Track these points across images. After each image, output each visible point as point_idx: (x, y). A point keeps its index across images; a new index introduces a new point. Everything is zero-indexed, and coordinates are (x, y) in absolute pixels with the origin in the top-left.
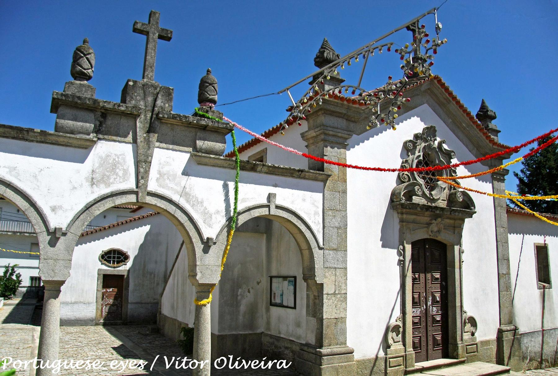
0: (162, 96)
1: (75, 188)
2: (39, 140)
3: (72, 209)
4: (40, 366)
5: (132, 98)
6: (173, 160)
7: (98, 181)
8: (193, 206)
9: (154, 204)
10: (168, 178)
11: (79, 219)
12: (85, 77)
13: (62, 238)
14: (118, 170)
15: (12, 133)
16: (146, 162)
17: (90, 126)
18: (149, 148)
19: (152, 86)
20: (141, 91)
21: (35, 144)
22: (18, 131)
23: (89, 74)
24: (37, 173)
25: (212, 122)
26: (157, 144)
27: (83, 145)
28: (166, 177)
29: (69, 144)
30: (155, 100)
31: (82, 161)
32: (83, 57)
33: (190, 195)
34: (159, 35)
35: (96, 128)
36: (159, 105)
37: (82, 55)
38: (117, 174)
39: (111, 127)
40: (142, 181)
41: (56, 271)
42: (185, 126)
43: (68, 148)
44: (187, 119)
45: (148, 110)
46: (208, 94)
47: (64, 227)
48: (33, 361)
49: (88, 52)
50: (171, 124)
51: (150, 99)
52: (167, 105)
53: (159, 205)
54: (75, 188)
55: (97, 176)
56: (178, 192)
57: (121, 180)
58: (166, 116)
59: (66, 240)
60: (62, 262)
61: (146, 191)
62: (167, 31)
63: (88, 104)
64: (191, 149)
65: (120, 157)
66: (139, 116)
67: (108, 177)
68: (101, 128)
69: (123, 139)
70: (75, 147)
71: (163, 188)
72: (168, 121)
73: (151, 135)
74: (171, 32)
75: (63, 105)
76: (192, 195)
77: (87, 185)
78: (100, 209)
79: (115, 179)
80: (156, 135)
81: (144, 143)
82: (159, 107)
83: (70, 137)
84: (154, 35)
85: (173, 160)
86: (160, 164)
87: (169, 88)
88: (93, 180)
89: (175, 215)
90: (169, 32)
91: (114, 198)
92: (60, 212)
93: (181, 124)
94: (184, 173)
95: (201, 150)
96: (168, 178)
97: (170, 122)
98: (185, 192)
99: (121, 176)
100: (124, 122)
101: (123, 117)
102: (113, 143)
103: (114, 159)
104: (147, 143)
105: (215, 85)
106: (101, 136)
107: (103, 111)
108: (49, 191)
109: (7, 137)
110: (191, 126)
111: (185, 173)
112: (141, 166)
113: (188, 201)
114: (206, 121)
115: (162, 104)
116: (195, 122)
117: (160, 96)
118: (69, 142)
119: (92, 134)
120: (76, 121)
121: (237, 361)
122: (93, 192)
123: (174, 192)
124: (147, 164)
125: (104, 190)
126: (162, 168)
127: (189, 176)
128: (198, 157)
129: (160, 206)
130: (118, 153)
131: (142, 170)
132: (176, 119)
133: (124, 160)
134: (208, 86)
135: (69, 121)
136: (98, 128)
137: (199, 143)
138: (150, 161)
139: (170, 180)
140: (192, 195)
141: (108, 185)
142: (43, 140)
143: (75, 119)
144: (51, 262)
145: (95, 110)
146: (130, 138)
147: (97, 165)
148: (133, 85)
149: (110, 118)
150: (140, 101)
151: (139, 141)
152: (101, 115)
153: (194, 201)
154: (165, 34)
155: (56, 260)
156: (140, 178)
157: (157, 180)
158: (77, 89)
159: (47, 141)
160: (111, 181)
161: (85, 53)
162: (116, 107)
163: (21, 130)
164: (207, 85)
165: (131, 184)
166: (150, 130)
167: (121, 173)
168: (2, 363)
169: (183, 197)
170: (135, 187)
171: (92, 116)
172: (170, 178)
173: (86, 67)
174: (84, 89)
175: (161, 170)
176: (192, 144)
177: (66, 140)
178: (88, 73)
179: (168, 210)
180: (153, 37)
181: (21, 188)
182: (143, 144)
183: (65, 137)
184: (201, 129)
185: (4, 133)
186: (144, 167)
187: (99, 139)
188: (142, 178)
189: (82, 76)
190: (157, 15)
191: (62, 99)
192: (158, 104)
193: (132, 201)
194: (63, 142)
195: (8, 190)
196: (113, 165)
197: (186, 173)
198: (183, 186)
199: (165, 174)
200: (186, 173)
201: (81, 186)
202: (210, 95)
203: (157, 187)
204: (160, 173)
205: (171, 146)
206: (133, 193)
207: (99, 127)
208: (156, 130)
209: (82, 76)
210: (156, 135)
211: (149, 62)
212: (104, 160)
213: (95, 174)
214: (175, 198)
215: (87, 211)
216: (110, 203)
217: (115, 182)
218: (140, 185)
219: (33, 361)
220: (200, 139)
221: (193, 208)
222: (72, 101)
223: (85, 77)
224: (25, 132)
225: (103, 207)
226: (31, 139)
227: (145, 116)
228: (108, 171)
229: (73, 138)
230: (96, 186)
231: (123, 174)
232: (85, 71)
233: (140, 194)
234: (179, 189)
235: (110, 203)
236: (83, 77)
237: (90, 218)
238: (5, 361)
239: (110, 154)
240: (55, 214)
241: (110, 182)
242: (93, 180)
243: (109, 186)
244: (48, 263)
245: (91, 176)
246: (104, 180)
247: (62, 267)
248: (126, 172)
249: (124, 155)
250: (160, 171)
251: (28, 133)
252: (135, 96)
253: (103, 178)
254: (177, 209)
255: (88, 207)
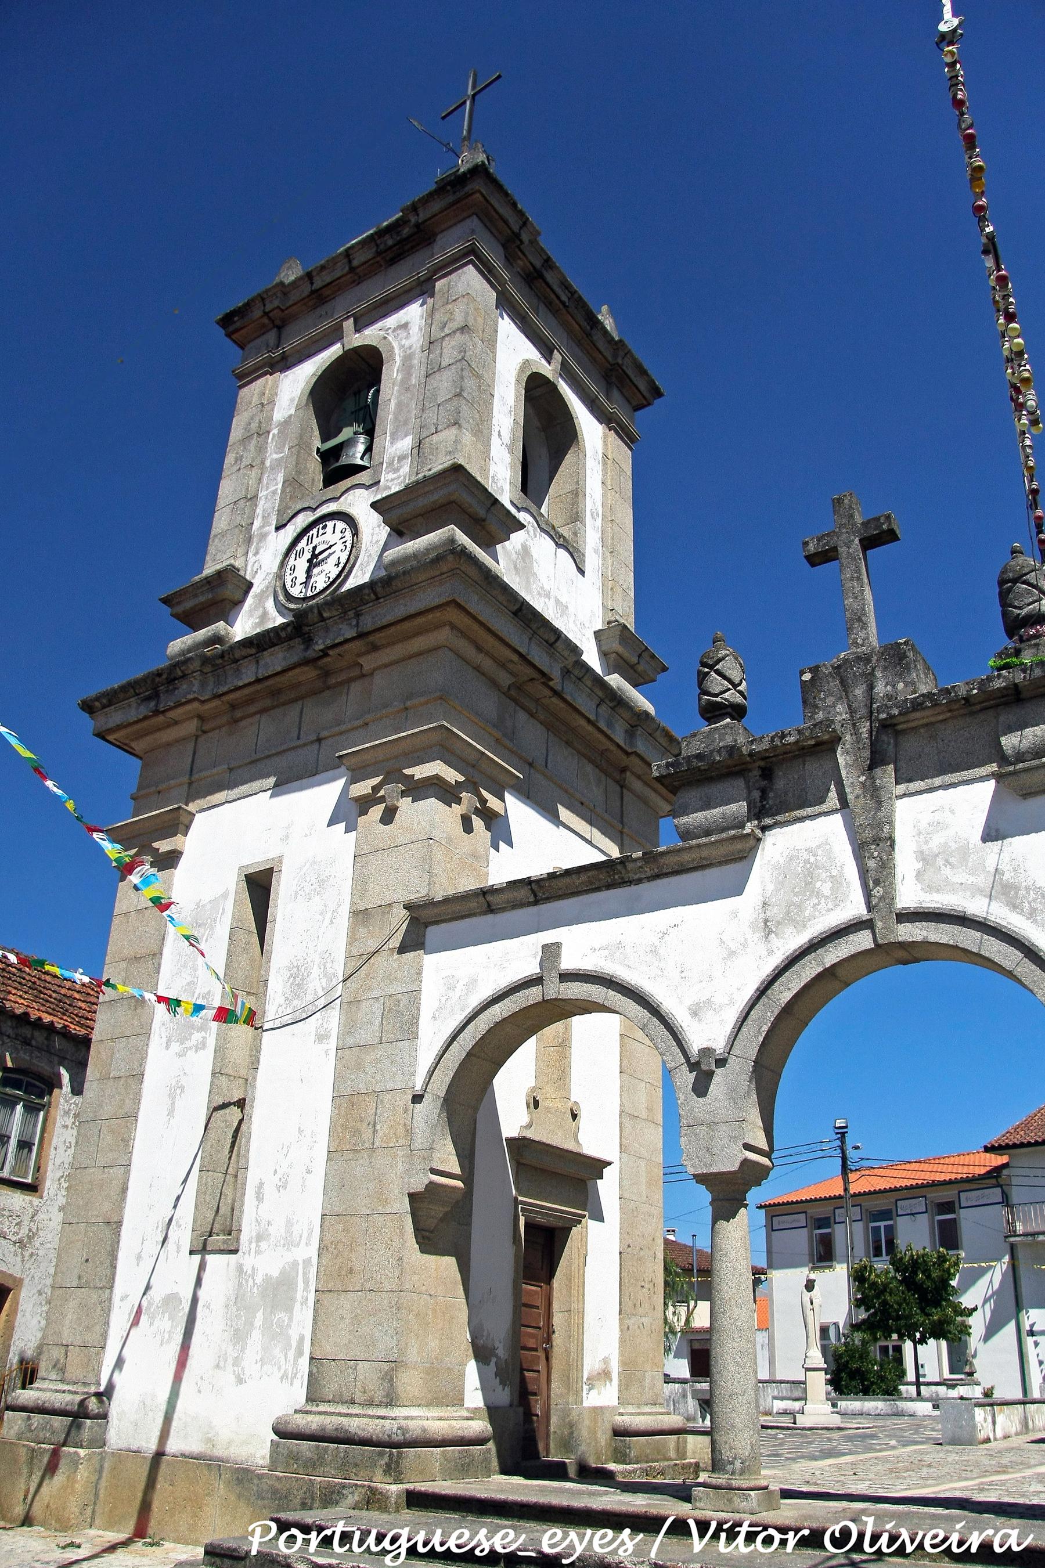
0: (885, 668)
1: (732, 953)
2: (649, 874)
3: (732, 1002)
4: (351, 1544)
5: (816, 707)
6: (952, 812)
7: (779, 923)
8: (1032, 915)
9: (919, 939)
10: (947, 861)
11: (749, 1021)
12: (723, 711)
13: (719, 1071)
14: (818, 884)
15: (601, 876)
16: (878, 842)
17: (740, 807)
18: (879, 803)
19: (859, 659)
20: (832, 684)
21: (645, 886)
22: (608, 870)
23: (728, 701)
24: (657, 943)
25: (1024, 671)
26: (901, 788)
27: (733, 854)
28: (940, 862)
29: (705, 863)
30: (871, 687)
31: (738, 890)
32: (709, 673)
33: (1017, 889)
34: (860, 540)
35: (755, 807)
36: (881, 695)
37: (706, 670)
38: (819, 894)
39: (786, 793)
40: (878, 891)
41: (715, 1151)
42: (965, 715)
43: (708, 872)
44: (953, 694)
45: (861, 718)
46: (1015, 607)
47: (719, 1045)
48: (334, 1532)
49: (715, 659)
50: (927, 725)
51: (859, 691)
52: (901, 686)
53: (933, 938)
54: (732, 953)
55: (774, 912)
56: (980, 891)
57: (830, 906)
58: (896, 711)
59: (726, 1076)
60: (724, 1127)
61: (891, 912)
62: (878, 519)
63: (719, 761)
64: (995, 765)
65: (820, 853)
66: (840, 739)
67: (800, 907)
68: (764, 803)
69: (817, 809)
70: (720, 864)
71: (938, 891)
72: (908, 721)
73: (878, 771)
74: (888, 517)
75: (684, 785)
76: (1024, 884)
77: (755, 938)
78: (790, 986)
79: (814, 905)
80: (891, 768)
81: (865, 796)
82: (883, 698)
83: (699, 846)
84: (849, 547)
85: (952, 812)
86: (920, 833)
87: (896, 643)
88: (768, 924)
89: (983, 953)
90: (882, 520)
91: (820, 951)
92: (708, 1015)
93: (949, 714)
94: (988, 835)
95: (1020, 757)
96: (947, 861)
97: (921, 722)
98: (1001, 884)
99: (828, 895)
100: (813, 768)
101: (808, 758)
102: (798, 826)
103: (807, 862)
104: (872, 796)
105: (1031, 577)
106: (768, 821)
107: (762, 763)
108: (683, 975)
109: (598, 889)
110: (978, 707)
111: (992, 834)
112: (867, 854)
113: (1014, 906)
114: (1005, 677)
115: (889, 688)
116: (975, 691)
117: (879, 674)
118: (703, 856)
119: (749, 824)
120: (709, 809)
121: (724, 1530)
122: (771, 952)
123: (969, 893)
124: (881, 844)
125: (795, 940)
126: (926, 842)
127: (1003, 838)
128: (1011, 778)
129: (937, 940)
130: (814, 845)
131: (872, 864)
132: (923, 709)
133: (829, 854)
134: (1011, 587)
135: (696, 815)
136: (759, 804)
137: (1010, 742)
138: (887, 836)
139: (953, 867)
140: (1024, 884)
141: (801, 925)
142: (656, 871)
143: (707, 806)
144: (702, 1130)
145: (744, 770)
146: (833, 799)
147: (771, 887)
148: (812, 677)
149: (781, 773)
150: (834, 706)
151: (850, 797)
152: (760, 776)
153: (1034, 900)
154: (875, 530)
155: (711, 1125)
156: (871, 884)
157: (919, 875)
158: (704, 742)
159: (664, 871)
160: (807, 913)
161: (710, 662)
162: (777, 742)
163: (612, 866)
164: (1007, 588)
165: (855, 907)
166: (876, 761)
167: (826, 889)
168: (250, 1538)
169: (996, 898)
170: (865, 912)
171: (740, 783)
172: (951, 860)
173: (716, 690)
174: (717, 736)
175: (925, 847)
176: (993, 751)
177: (695, 855)
178: (726, 699)
179: (961, 946)
180: (848, 552)
181: (633, 983)
182: (862, 800)
183: (691, 848)
184: (1006, 704)
185: (590, 882)
186: (876, 854)
187: (764, 829)
188: (877, 883)
189: (717, 713)
190: (846, 501)
191: (669, 774)
192: (879, 693)
193: (864, 948)
194: (693, 860)
195: (611, 993)
196: (805, 877)
197: (994, 834)
198: (993, 870)
199: (937, 855)
200: (994, 834)
201: (745, 945)
202: (1020, 608)
203: (922, 893)
204: (923, 857)
205: (937, 781)
206: (863, 926)
207: (761, 802)
208: (888, 755)
209: (717, 713)
210: (891, 768)
211: (852, 611)
212: (782, 873)
213: (770, 908)
214: (976, 907)
215: (764, 999)
216: (811, 966)
217: (817, 913)
218: (874, 901)
219: (334, 1532)
220: (1010, 729)
221: (1035, 921)
222: (689, 769)
223: (723, 711)
224: (619, 867)
225: (797, 980)
226: (636, 877)
227: (856, 733)
228: (796, 895)
229: (706, 845)
230: (776, 935)
231: (832, 888)
232: (718, 699)
233: (879, 924)
234: (983, 881)
235: (811, 966)
236: (721, 712)
237: (772, 1012)
238: (258, 1531)
239: (795, 853)
240: (700, 1020)
241: (804, 918)
242: (768, 924)
243: (805, 926)
244: (696, 1135)
245: (762, 916)
246: (793, 917)
247: (726, 1141)
248: (837, 881)
249: (827, 844)
250: (922, 852)
251: (625, 867)
252: (820, 699)
253: (788, 913)
254: (986, 937)
255: (762, 991)
